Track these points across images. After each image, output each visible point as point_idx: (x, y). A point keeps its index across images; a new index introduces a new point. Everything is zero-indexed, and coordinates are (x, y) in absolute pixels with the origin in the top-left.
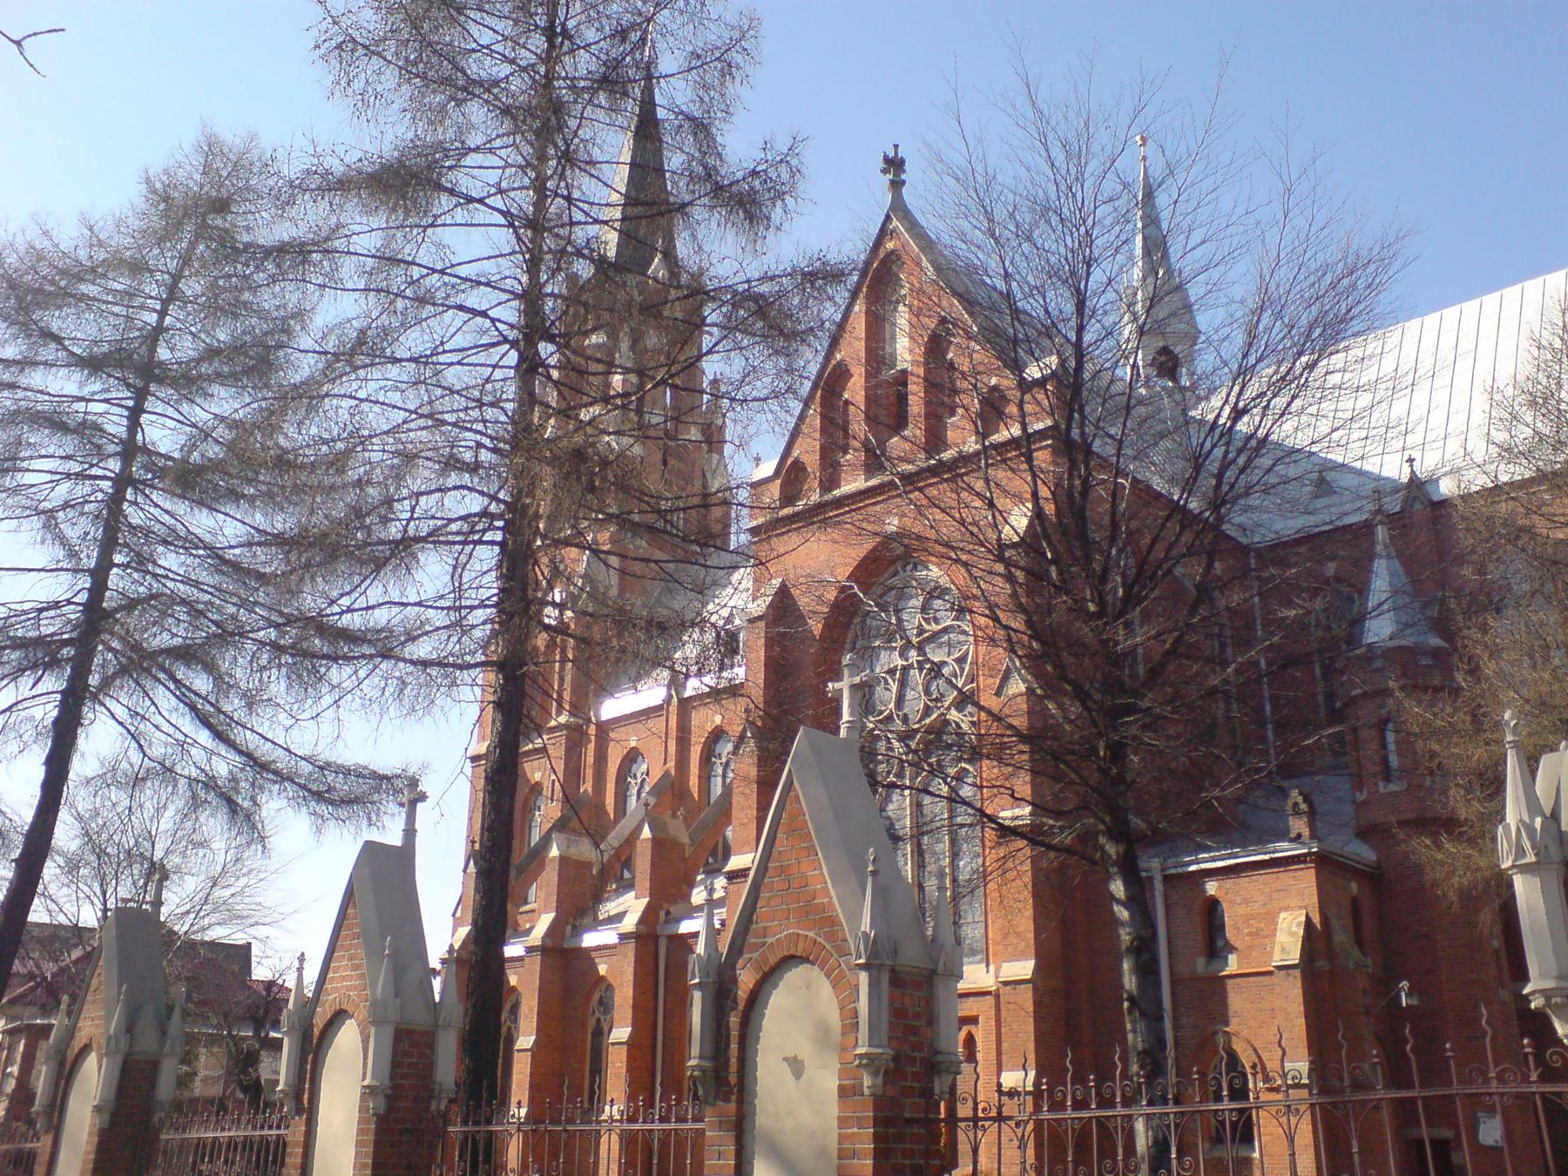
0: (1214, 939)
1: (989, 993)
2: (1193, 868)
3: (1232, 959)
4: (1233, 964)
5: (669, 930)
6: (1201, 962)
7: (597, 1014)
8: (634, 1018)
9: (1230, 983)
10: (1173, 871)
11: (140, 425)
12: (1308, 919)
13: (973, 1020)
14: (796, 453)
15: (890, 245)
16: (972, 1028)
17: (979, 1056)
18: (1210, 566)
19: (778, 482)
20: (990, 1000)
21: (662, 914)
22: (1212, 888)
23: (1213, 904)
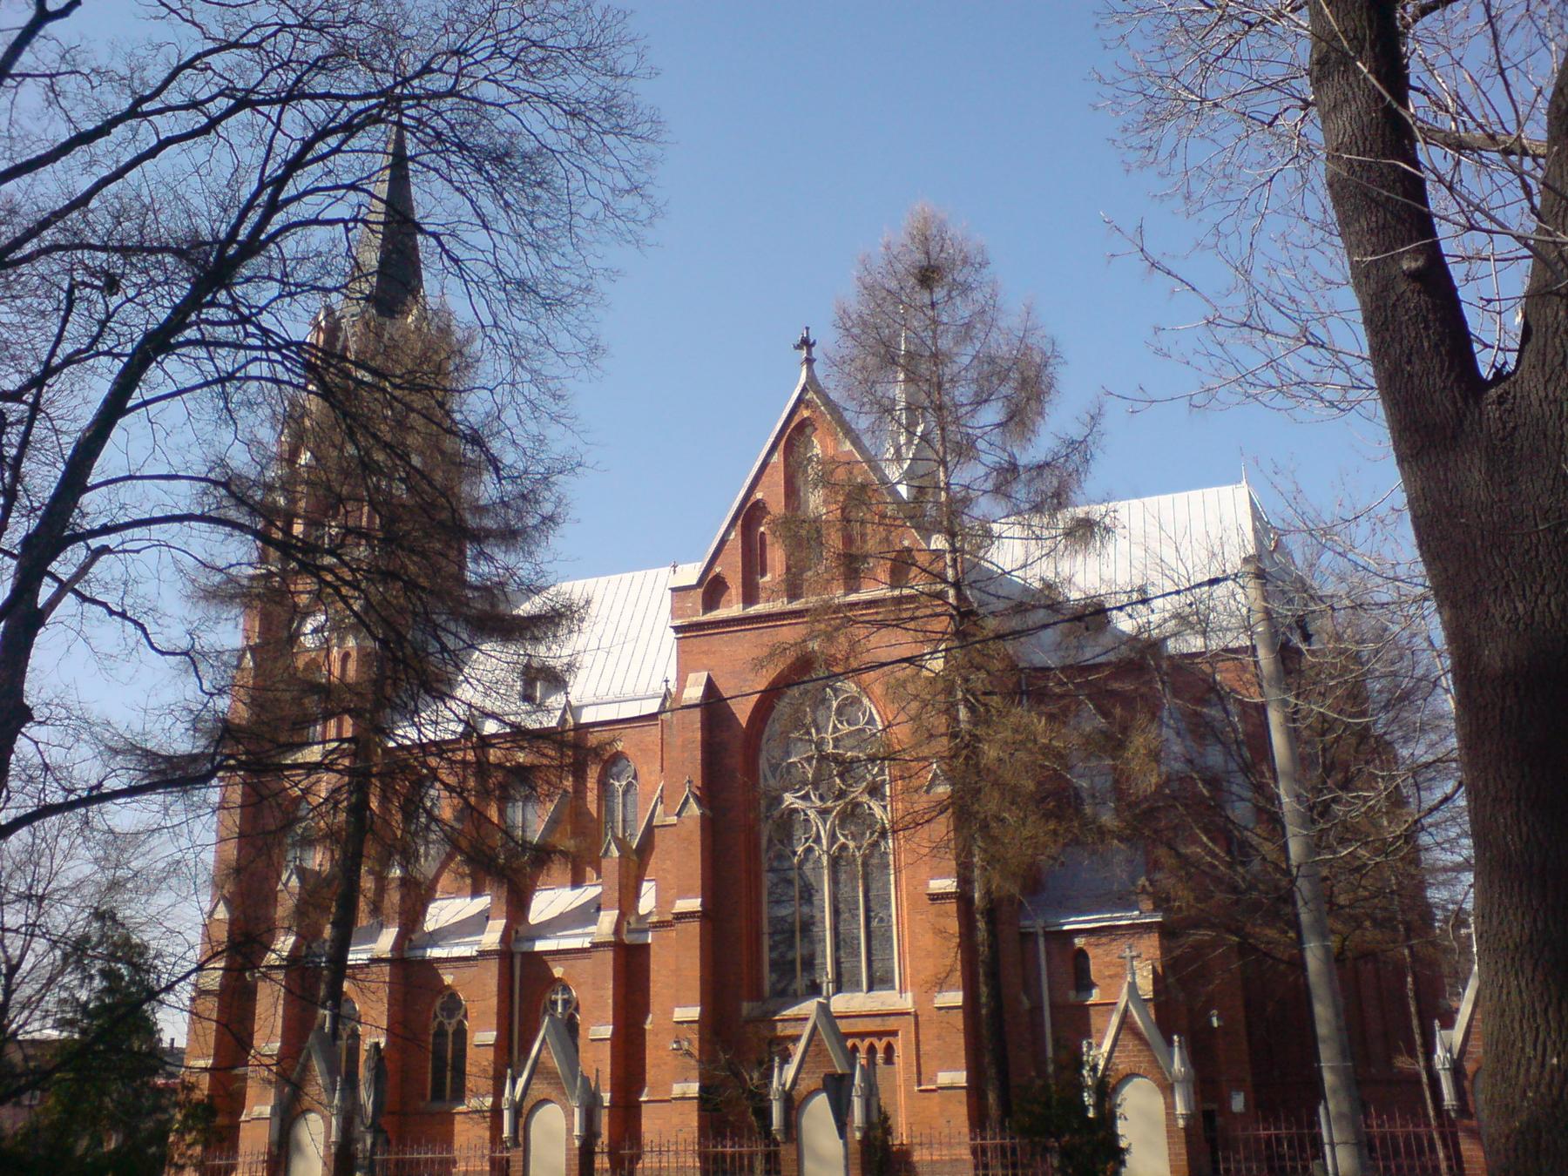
0: (1084, 983)
1: (908, 1014)
2: (1066, 928)
3: (1095, 992)
4: (1095, 996)
5: (525, 947)
6: (1072, 995)
7: (440, 1018)
8: (498, 1024)
9: (1092, 1011)
10: (1052, 929)
11: (879, 629)
12: (1154, 968)
13: (894, 1033)
14: (717, 569)
15: (806, 413)
16: (891, 1039)
17: (896, 1060)
18: (277, 527)
19: (700, 591)
20: (912, 1019)
21: (513, 933)
22: (1079, 942)
23: (1082, 955)
